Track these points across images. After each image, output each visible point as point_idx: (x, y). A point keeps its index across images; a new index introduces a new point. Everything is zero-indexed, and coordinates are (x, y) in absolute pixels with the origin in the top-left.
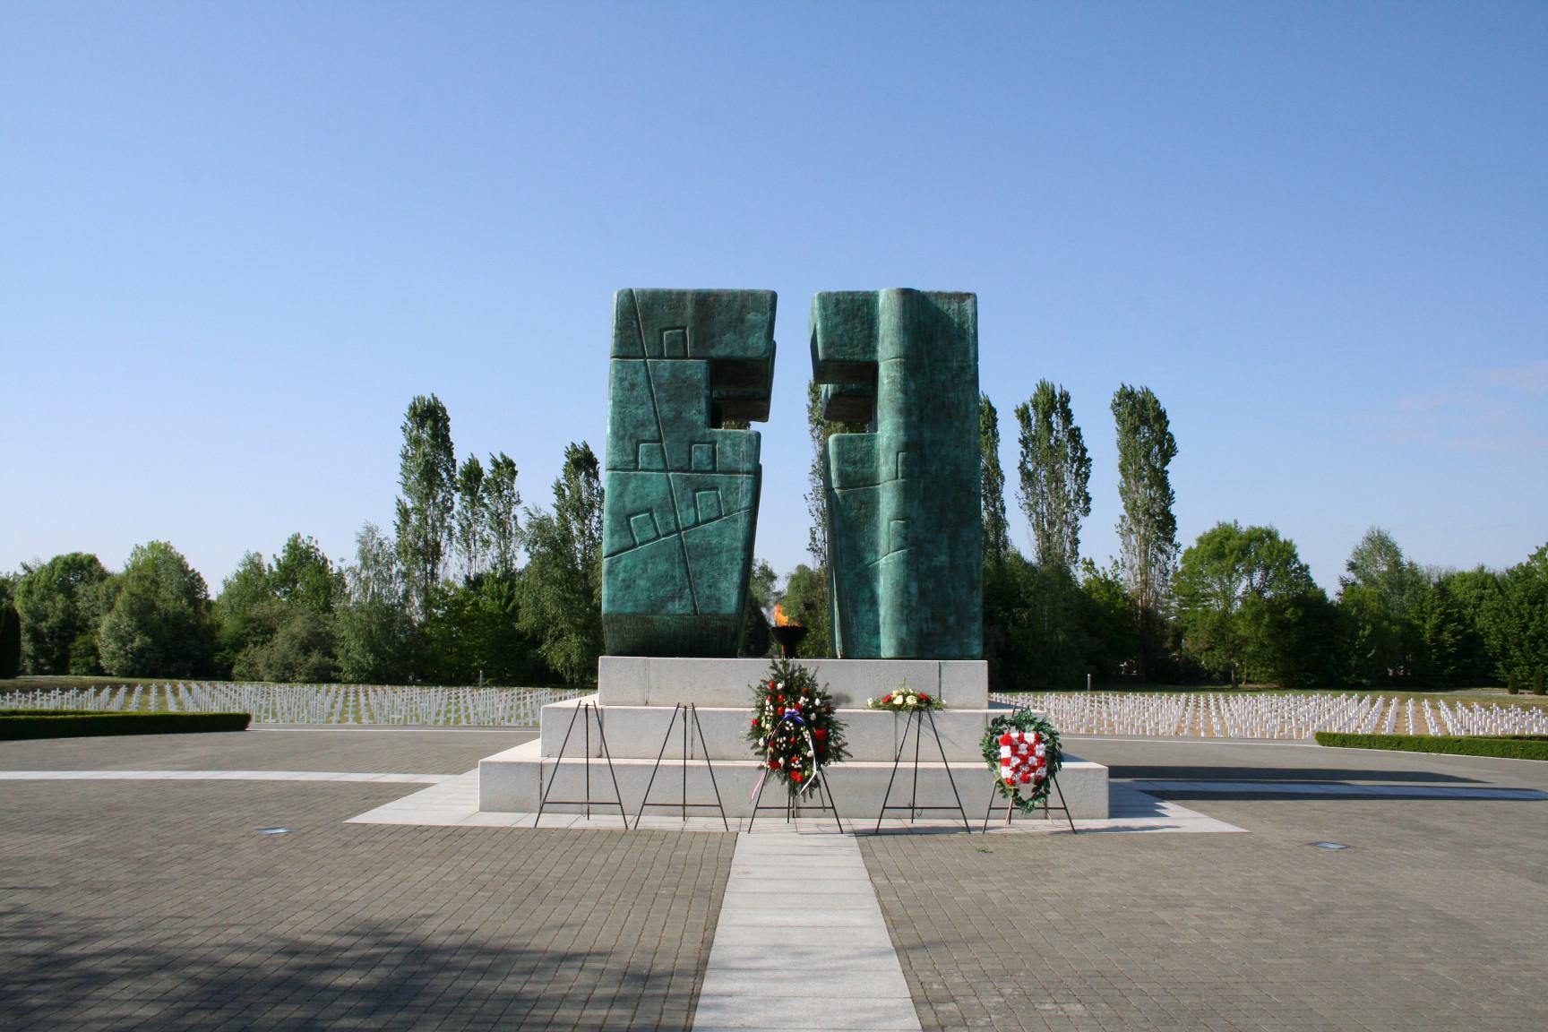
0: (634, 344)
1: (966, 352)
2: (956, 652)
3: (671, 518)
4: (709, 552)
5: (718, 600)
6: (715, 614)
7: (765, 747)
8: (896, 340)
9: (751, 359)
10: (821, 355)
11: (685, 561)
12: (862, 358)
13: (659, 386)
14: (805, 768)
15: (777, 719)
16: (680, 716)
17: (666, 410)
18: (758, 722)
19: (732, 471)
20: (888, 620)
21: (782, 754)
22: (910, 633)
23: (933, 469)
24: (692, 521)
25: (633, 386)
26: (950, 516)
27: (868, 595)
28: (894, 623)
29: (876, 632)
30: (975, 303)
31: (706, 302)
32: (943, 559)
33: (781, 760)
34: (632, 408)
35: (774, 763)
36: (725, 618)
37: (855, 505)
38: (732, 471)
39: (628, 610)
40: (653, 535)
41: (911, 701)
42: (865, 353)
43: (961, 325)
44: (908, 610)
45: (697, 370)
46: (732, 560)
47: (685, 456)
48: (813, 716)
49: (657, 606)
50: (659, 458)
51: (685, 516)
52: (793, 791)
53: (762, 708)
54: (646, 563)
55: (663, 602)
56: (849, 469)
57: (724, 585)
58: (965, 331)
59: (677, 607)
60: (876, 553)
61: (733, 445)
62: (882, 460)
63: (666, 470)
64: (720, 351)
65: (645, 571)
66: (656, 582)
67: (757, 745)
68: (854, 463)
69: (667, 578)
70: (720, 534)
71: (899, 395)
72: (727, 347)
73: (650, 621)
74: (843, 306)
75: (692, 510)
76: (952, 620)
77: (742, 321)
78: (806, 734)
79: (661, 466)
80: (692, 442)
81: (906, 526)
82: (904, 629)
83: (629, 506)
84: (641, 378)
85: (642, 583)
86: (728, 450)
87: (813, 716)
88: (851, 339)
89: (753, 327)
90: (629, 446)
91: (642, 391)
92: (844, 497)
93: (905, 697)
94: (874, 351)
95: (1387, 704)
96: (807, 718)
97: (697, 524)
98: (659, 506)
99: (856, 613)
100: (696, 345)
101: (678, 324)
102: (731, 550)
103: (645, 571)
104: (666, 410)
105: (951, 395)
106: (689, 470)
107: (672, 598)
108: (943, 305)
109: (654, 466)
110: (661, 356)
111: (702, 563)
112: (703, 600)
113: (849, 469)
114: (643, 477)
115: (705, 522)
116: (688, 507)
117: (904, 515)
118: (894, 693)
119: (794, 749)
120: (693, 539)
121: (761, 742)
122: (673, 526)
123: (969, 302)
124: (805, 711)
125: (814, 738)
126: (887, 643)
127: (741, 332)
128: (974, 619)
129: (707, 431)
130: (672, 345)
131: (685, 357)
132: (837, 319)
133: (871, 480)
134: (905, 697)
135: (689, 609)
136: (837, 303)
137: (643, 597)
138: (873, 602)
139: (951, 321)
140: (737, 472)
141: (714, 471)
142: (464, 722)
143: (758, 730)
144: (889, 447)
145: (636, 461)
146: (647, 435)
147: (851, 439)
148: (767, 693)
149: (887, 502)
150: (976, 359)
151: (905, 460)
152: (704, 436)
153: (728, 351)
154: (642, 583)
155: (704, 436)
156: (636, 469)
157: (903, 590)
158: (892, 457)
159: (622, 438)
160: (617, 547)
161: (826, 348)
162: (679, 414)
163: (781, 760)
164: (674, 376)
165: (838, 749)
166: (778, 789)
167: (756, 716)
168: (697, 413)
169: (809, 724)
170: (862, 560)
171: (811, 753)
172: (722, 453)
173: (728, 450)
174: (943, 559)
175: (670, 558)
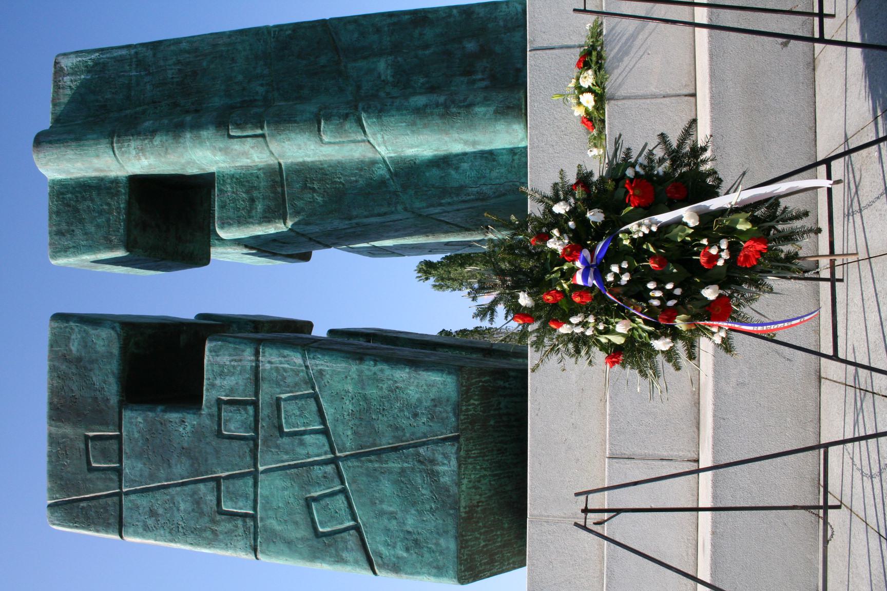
0: (105, 509)
1: (120, 60)
3: (318, 471)
4: (365, 414)
5: (436, 402)
6: (457, 410)
7: (675, 334)
8: (92, 151)
9: (124, 349)
10: (120, 253)
11: (379, 453)
12: (123, 198)
13: (152, 478)
14: (730, 232)
15: (604, 307)
17: (180, 469)
18: (615, 353)
19: (256, 377)
20: (468, 136)
21: (691, 293)
22: (486, 101)
23: (261, 90)
24: (322, 439)
25: (153, 513)
26: (323, 60)
27: (435, 172)
28: (471, 127)
29: (489, 156)
30: (65, 55)
31: (63, 409)
32: (382, 66)
33: (710, 293)
34: (178, 517)
35: (721, 310)
36: (465, 393)
37: (308, 196)
38: (256, 377)
39: (453, 546)
40: (341, 498)
41: (588, 79)
42: (118, 193)
43: (89, 70)
44: (450, 107)
45: (135, 421)
46: (375, 379)
47: (236, 444)
48: (595, 216)
49: (444, 500)
50: (239, 483)
51: (314, 448)
52: (789, 267)
53: (579, 343)
54: (382, 513)
55: (440, 491)
56: (260, 207)
57: (413, 393)
58: (96, 63)
59: (447, 468)
60: (373, 163)
61: (222, 374)
62: (244, 162)
63: (255, 475)
64: (112, 391)
65: (392, 516)
66: (410, 500)
67: (670, 355)
68: (252, 200)
69: (402, 480)
70: (339, 397)
71: (157, 140)
72: (107, 382)
73: (471, 510)
74: (64, 227)
75: (308, 438)
76: (471, 46)
77: (79, 359)
78: (638, 228)
79: (250, 481)
80: (219, 434)
81: (328, 118)
82: (479, 110)
83: (303, 532)
84: (143, 502)
85: (411, 522)
86: (229, 382)
87: (595, 216)
88: (101, 213)
89: (85, 346)
91: (158, 501)
92: (297, 213)
93: (581, 90)
94: (115, 181)
96: (598, 232)
97: (325, 432)
98: (302, 487)
99: (461, 188)
100: (105, 424)
101: (82, 446)
102: (361, 382)
103: (392, 516)
104: (180, 469)
106: (255, 440)
107: (433, 475)
108: (66, 96)
109: (250, 491)
110: (119, 471)
111: (380, 426)
112: (436, 427)
113: (260, 207)
114: (264, 508)
115: (323, 421)
116: (302, 444)
117: (314, 123)
118: (579, 112)
119: (680, 259)
120: (346, 438)
121: (661, 345)
122: (330, 469)
123: (66, 63)
124: (582, 236)
125: (650, 209)
126: (501, 137)
127: (92, 362)
129: (205, 411)
130: (105, 456)
131: (119, 438)
132: (78, 232)
133: (277, 177)
134: (581, 90)
135: (450, 449)
136: (60, 233)
137: (432, 522)
138: (444, 162)
139: (84, 84)
140: (256, 370)
141: (255, 404)
143: (632, 353)
144: (225, 151)
145: (245, 516)
146: (211, 498)
147: (223, 207)
148: (545, 330)
149: (299, 149)
150: (128, 47)
151: (239, 126)
152: (211, 415)
153: (112, 380)
154: (411, 522)
155: (211, 415)
156: (254, 517)
157: (420, 115)
158: (236, 146)
159: (214, 532)
160: (361, 557)
161: (111, 247)
162: (186, 452)
163: (710, 293)
164: (139, 456)
165: (675, 156)
166: (777, 300)
167: (599, 356)
169: (613, 224)
170: (383, 182)
171: (687, 215)
172: (232, 391)
173: (229, 382)
174: (382, 66)
175: (373, 475)
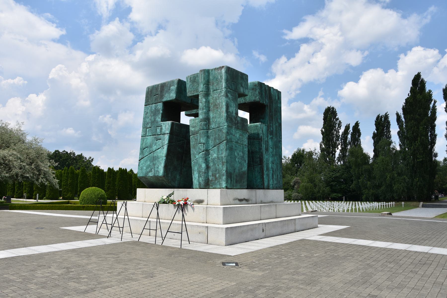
2: (239, 186)
16: (155, 205)
25: (147, 113)
36: (160, 177)
57: (160, 167)
64: (165, 100)
90: (145, 129)
95: (349, 203)
105: (218, 101)
126: (195, 182)
128: (223, 175)
142: (305, 211)
146: (148, 126)
168: (159, 118)
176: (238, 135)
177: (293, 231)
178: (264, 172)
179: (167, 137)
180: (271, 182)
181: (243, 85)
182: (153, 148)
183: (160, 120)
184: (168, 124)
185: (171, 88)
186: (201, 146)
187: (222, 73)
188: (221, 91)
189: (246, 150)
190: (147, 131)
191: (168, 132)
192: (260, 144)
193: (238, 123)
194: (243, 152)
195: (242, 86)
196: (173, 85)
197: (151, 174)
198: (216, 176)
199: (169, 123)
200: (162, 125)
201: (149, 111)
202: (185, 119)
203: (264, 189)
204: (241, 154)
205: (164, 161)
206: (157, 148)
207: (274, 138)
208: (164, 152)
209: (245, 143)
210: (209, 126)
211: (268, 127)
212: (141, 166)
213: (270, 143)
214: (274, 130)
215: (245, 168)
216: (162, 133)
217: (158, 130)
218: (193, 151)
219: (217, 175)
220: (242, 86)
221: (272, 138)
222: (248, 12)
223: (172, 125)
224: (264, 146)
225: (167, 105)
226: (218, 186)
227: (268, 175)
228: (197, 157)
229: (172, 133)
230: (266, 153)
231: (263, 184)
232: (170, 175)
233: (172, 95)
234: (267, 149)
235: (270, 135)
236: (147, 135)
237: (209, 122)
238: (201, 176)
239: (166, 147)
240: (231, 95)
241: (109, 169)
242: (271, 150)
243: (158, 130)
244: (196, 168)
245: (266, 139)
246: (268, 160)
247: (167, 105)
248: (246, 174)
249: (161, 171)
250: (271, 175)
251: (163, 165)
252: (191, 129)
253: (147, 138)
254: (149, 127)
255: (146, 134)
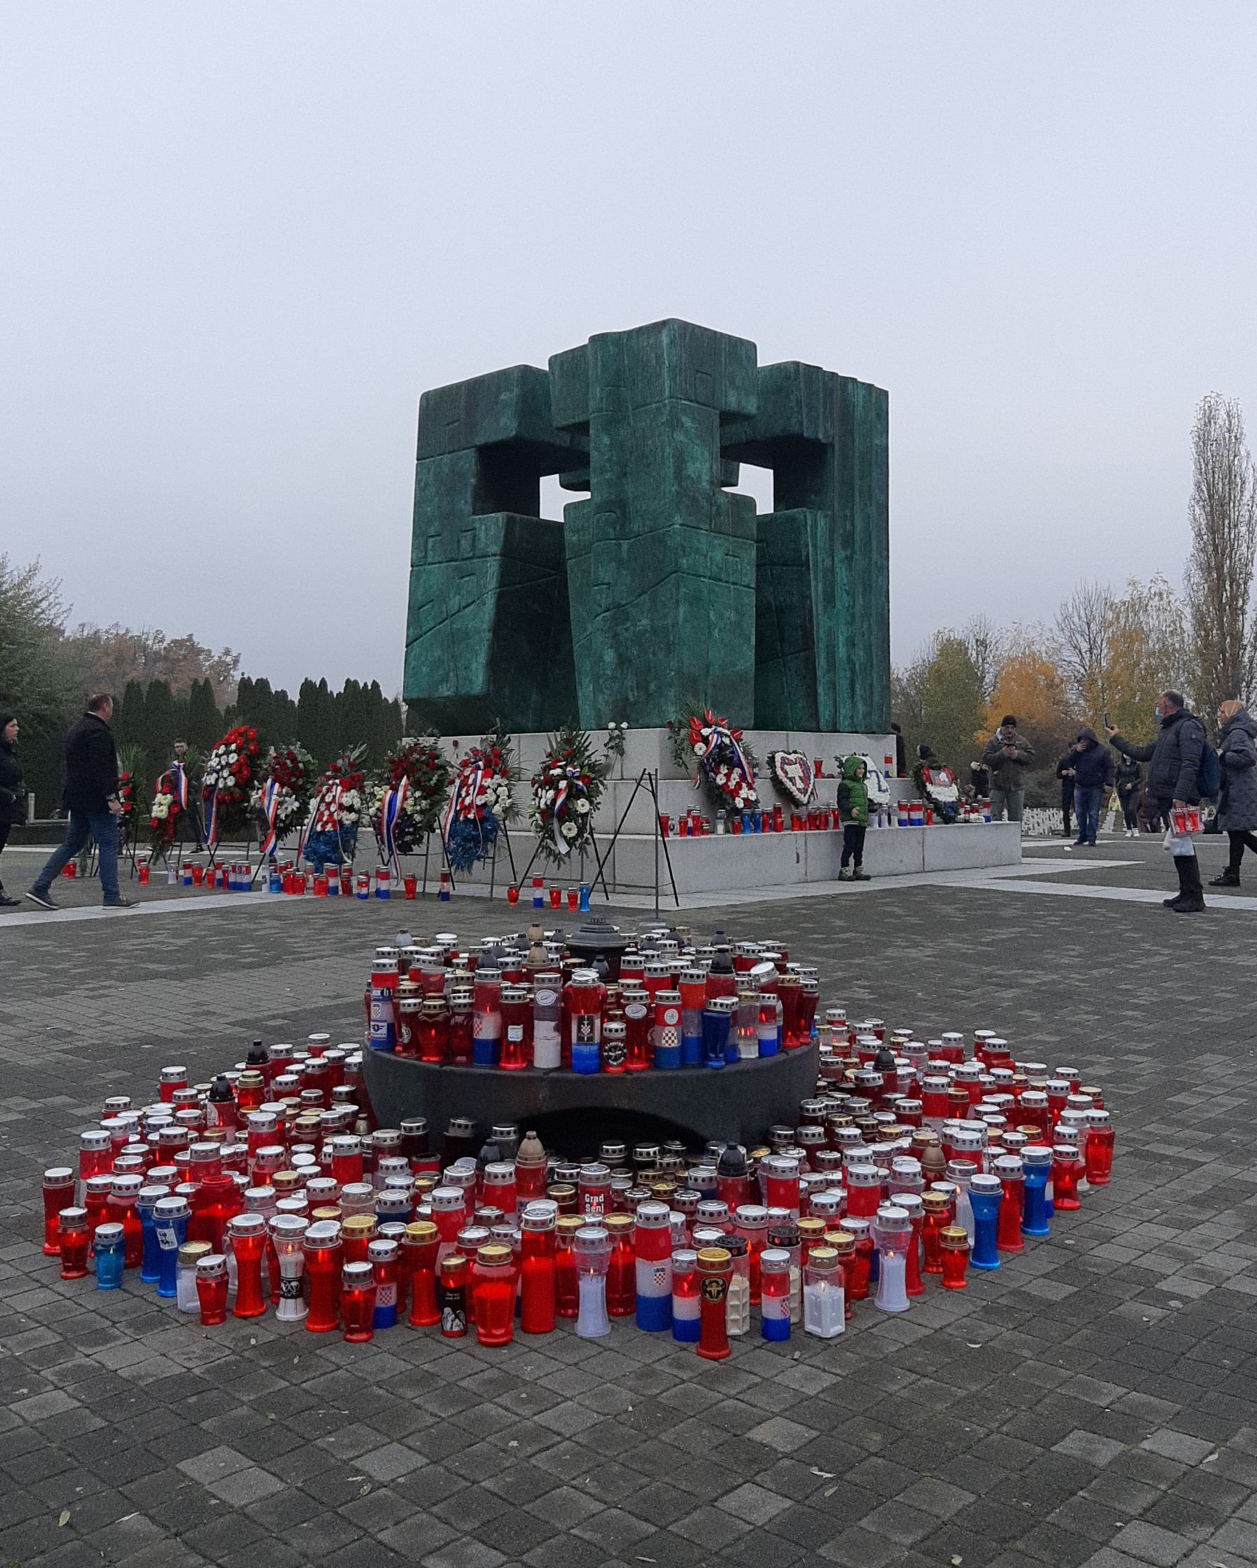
25: (426, 485)
57: (474, 666)
64: (480, 440)
146: (432, 531)
168: (465, 503)
176: (718, 556)
177: (913, 869)
178: (820, 673)
179: (493, 566)
180: (844, 711)
181: (738, 382)
182: (451, 602)
183: (468, 508)
184: (496, 524)
185: (503, 397)
186: (600, 592)
187: (661, 346)
188: (658, 409)
189: (750, 601)
190: (430, 545)
191: (495, 549)
192: (803, 580)
193: (718, 513)
194: (737, 610)
195: (732, 384)
196: (507, 390)
197: (445, 691)
198: (647, 689)
199: (500, 516)
200: (477, 525)
201: (431, 478)
202: (554, 499)
203: (818, 730)
204: (732, 615)
205: (486, 644)
206: (463, 604)
207: (857, 556)
208: (486, 613)
209: (746, 581)
210: (623, 526)
211: (833, 519)
212: (414, 663)
213: (842, 574)
214: (858, 530)
215: (746, 660)
216: (478, 553)
217: (465, 543)
218: (576, 611)
219: (652, 687)
220: (732, 384)
221: (849, 559)
222: (263, 683)
223: (510, 522)
224: (817, 589)
225: (488, 453)
226: (657, 721)
227: (833, 685)
228: (590, 629)
229: (508, 554)
230: (825, 608)
231: (816, 715)
232: (507, 692)
233: (505, 426)
234: (830, 599)
235: (844, 548)
236: (430, 560)
237: (624, 513)
238: (601, 691)
239: (490, 601)
240: (694, 419)
241: (307, 687)
242: (842, 600)
243: (465, 543)
244: (587, 666)
245: (828, 562)
246: (831, 634)
247: (488, 453)
248: (752, 682)
249: (478, 681)
250: (843, 685)
251: (482, 658)
252: (570, 538)
253: (430, 572)
254: (434, 532)
255: (425, 557)
